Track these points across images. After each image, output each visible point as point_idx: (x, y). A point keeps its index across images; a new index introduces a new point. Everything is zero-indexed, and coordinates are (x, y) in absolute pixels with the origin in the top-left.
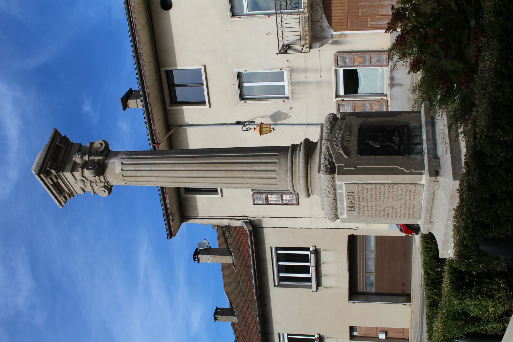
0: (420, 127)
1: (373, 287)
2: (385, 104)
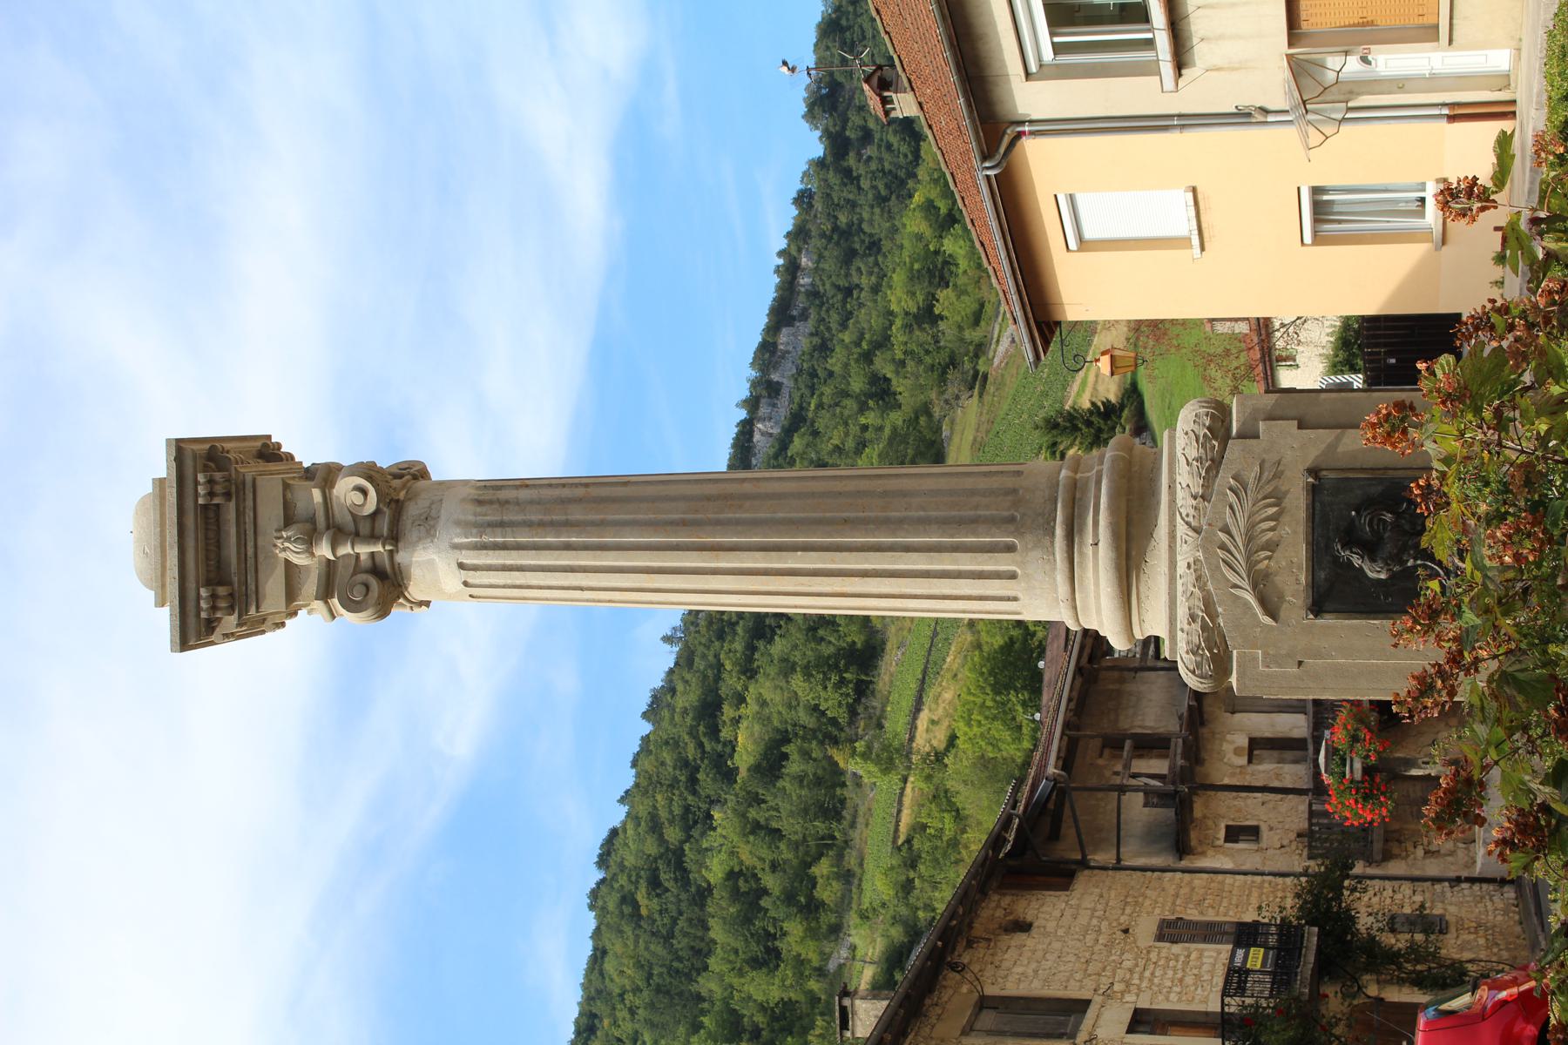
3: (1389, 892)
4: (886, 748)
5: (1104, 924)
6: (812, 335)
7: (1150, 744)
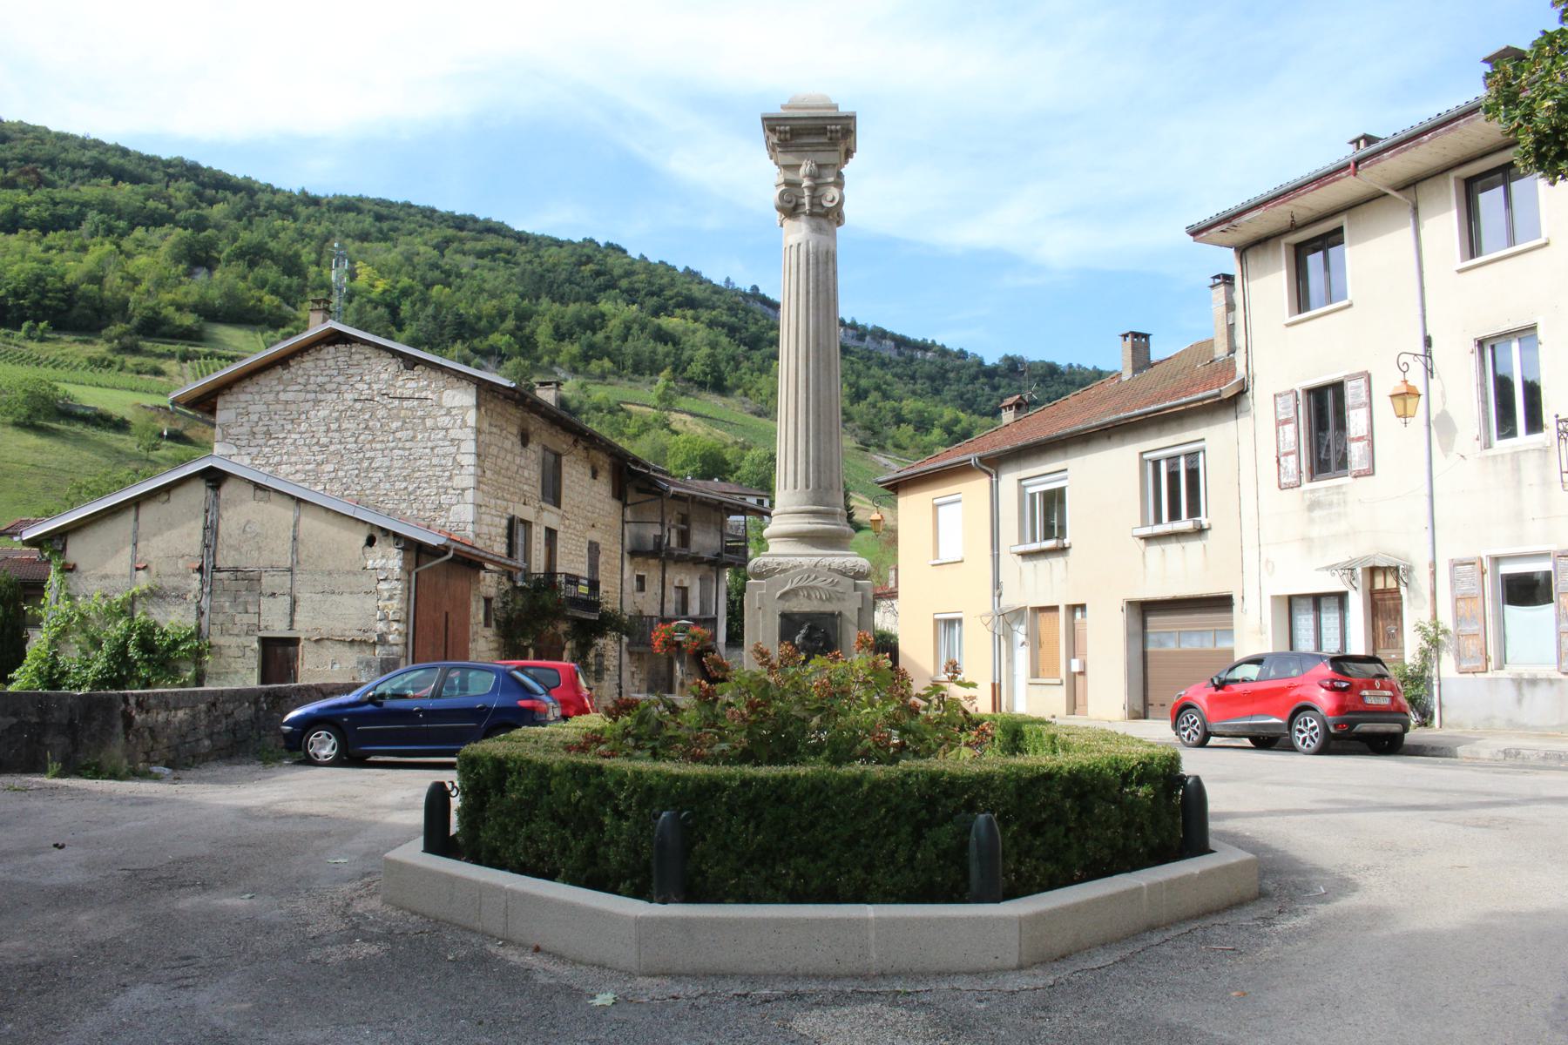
2: (1478, 667)
3: (614, 654)
4: (672, 398)
5: (596, 515)
6: (890, 358)
7: (684, 538)
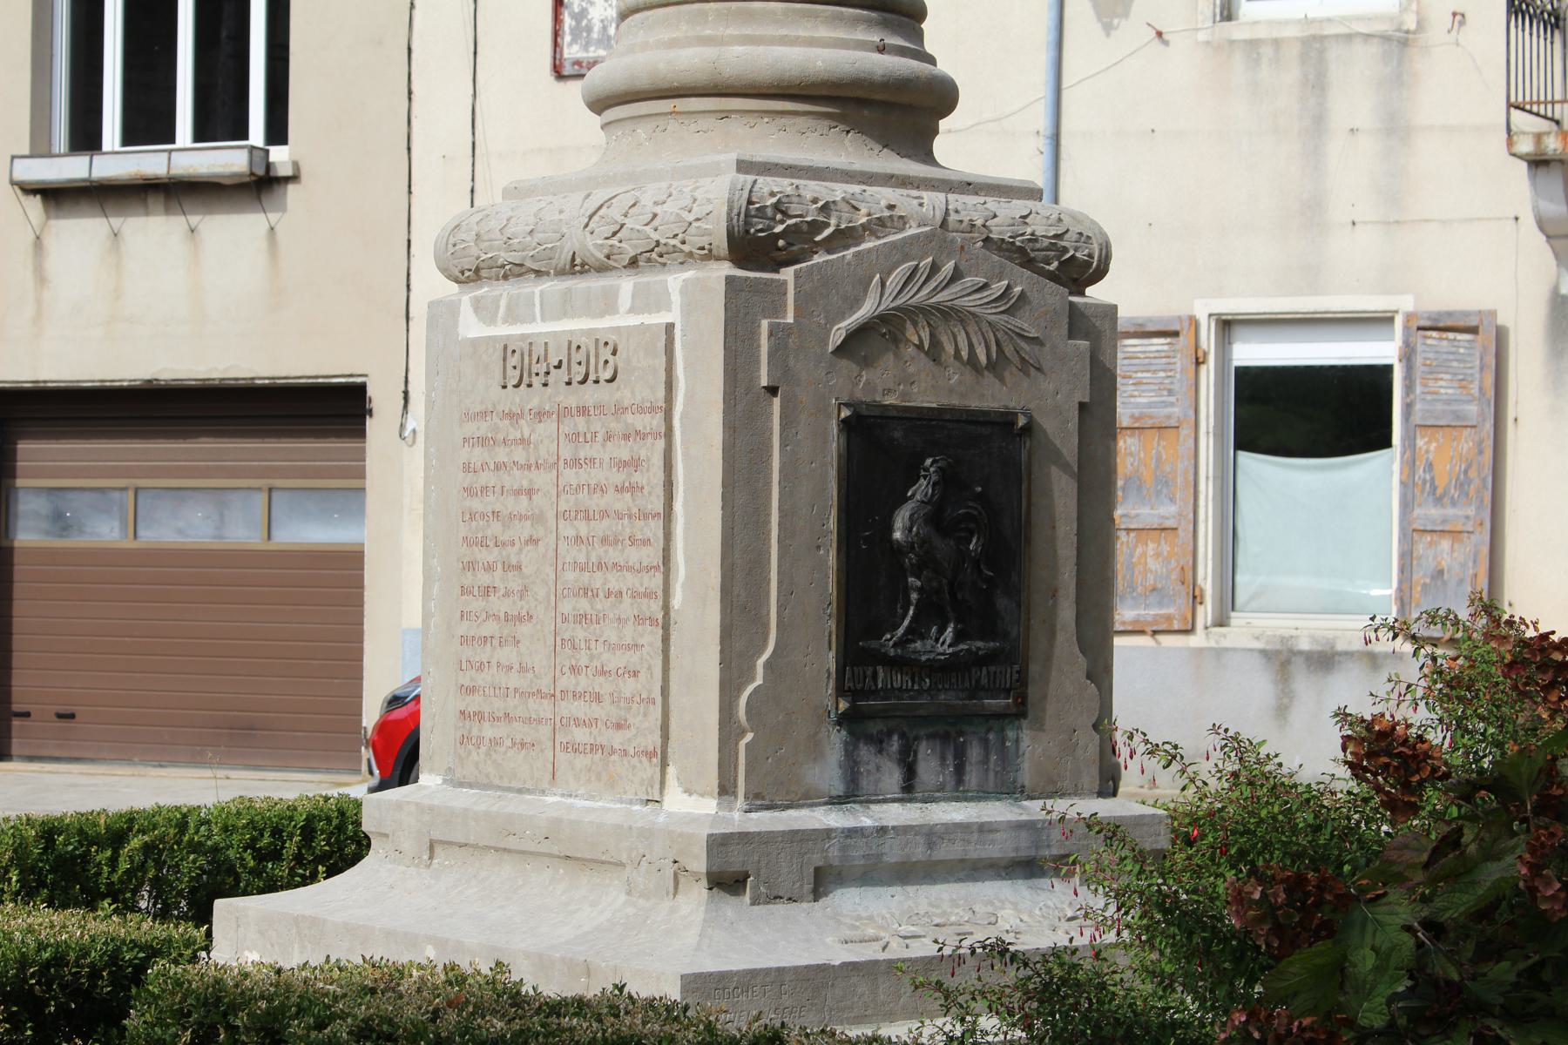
0: (1012, 790)
1: (47, 533)
2: (1169, 618)
